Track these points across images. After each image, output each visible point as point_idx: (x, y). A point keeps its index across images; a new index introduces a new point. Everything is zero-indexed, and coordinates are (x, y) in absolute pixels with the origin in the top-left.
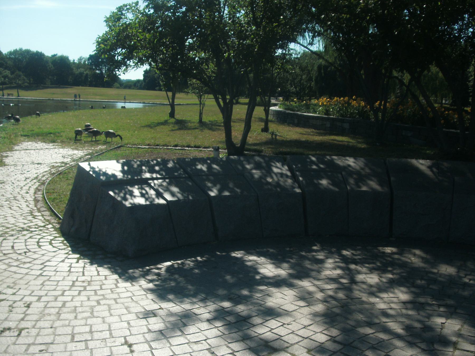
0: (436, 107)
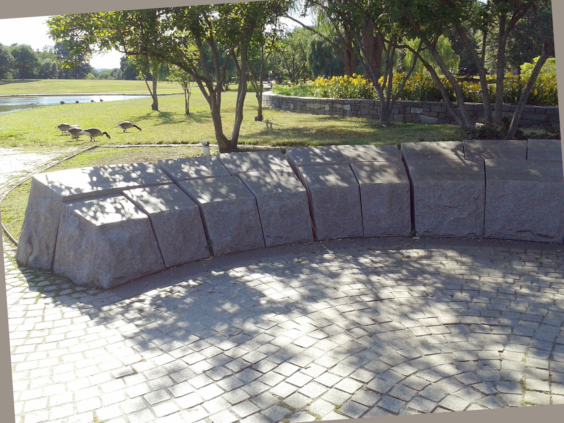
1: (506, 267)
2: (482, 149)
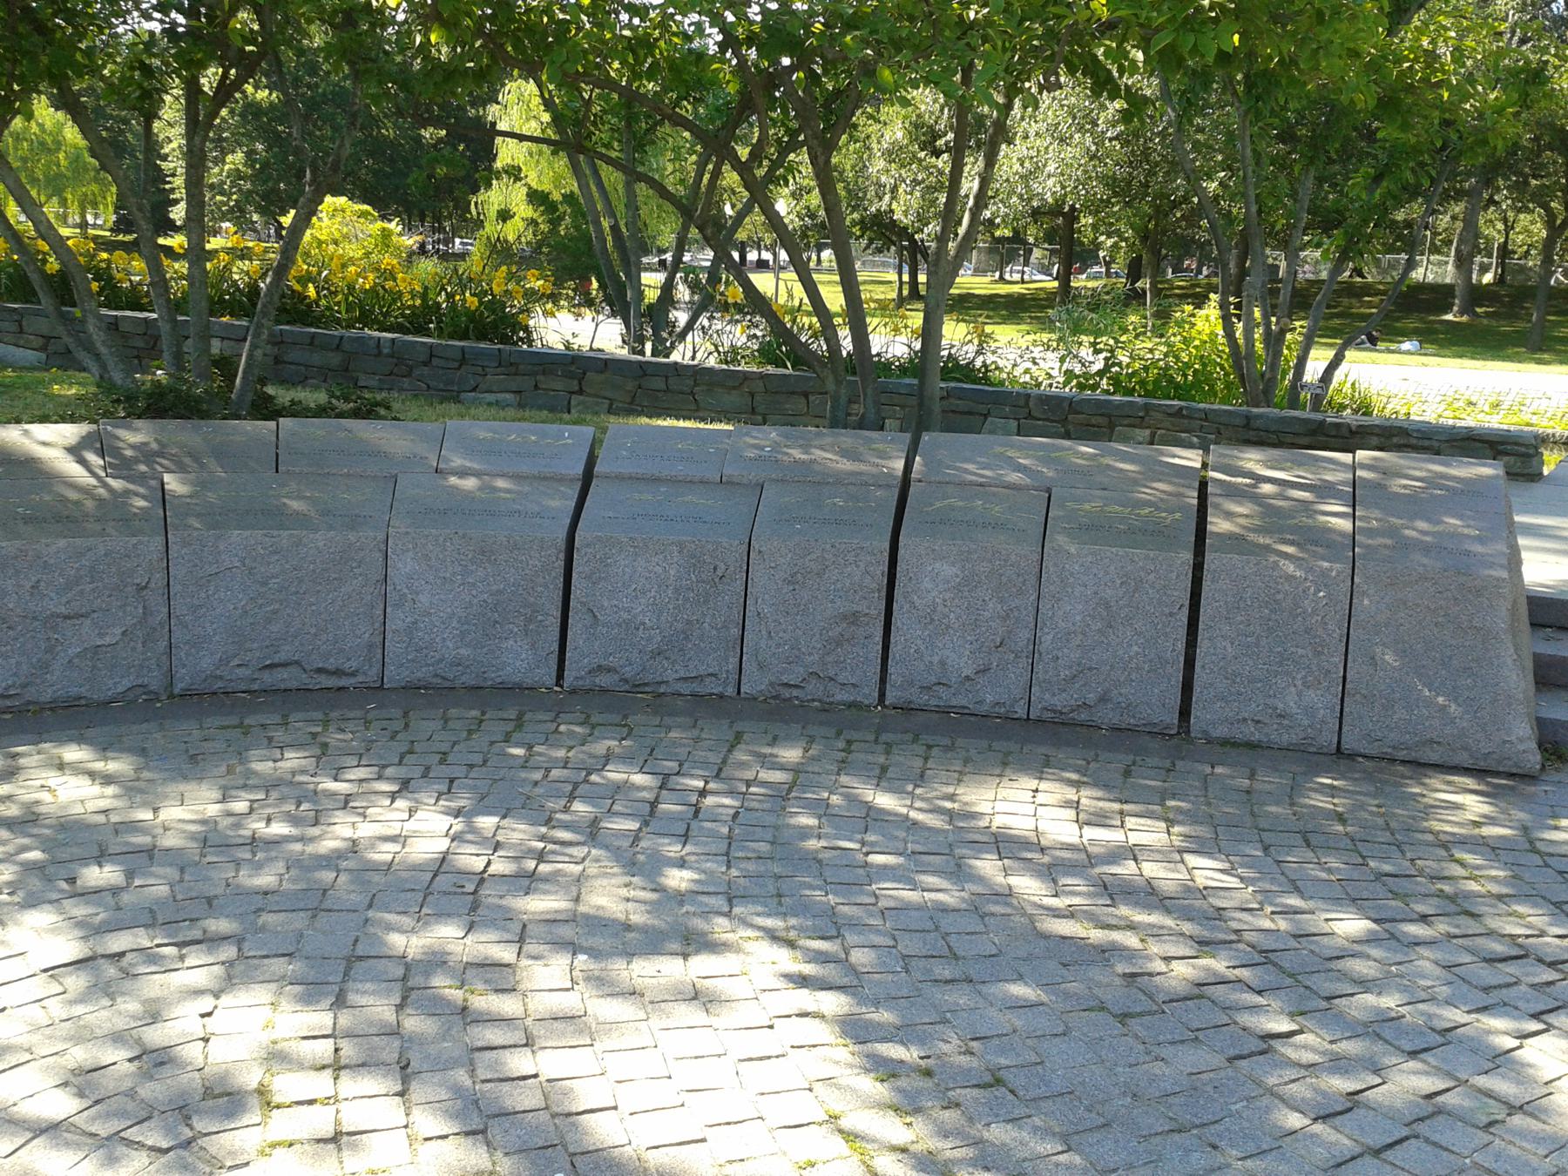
0: (68, 238)
1: (230, 771)
2: (154, 446)
